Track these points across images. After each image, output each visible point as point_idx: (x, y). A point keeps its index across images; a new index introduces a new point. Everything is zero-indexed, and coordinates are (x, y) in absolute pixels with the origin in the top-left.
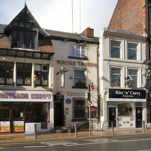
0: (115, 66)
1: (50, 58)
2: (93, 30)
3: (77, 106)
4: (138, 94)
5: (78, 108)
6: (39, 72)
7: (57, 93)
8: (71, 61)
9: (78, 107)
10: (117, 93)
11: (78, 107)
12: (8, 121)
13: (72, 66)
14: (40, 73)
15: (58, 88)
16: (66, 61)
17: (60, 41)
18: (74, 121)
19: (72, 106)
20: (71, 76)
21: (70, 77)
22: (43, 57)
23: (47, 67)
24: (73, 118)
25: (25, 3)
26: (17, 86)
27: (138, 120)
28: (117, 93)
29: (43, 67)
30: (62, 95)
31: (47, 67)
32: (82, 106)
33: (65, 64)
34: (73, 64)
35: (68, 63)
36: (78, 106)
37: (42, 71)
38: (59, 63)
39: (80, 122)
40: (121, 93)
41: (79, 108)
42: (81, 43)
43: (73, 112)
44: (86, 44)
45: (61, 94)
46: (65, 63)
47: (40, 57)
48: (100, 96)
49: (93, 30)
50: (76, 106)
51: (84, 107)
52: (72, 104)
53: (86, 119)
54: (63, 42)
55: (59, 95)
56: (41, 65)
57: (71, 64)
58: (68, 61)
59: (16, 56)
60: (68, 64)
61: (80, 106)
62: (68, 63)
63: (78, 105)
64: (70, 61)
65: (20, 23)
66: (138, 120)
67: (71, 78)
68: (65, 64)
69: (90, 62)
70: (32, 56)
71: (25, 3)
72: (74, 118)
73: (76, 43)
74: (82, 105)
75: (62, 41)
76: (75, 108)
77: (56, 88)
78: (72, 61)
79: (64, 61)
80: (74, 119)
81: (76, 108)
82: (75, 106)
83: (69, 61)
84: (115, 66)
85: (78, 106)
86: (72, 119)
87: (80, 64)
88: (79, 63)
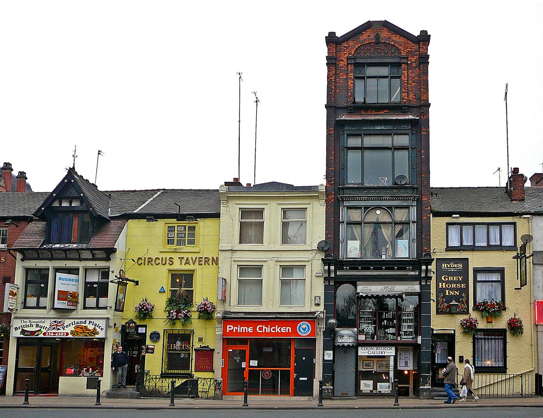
0: (237, 274)
3: (170, 345)
4: (289, 329)
5: (174, 350)
9: (173, 347)
10: (175, 348)
11: (173, 347)
12: (333, 266)
13: (168, 267)
14: (96, 286)
18: (164, 376)
25: (74, 164)
28: (175, 348)
34: (168, 262)
36: (173, 346)
51: (184, 348)
59: (51, 259)
60: (159, 263)
71: (74, 164)
84: (237, 274)
87: (184, 261)
88: (181, 262)
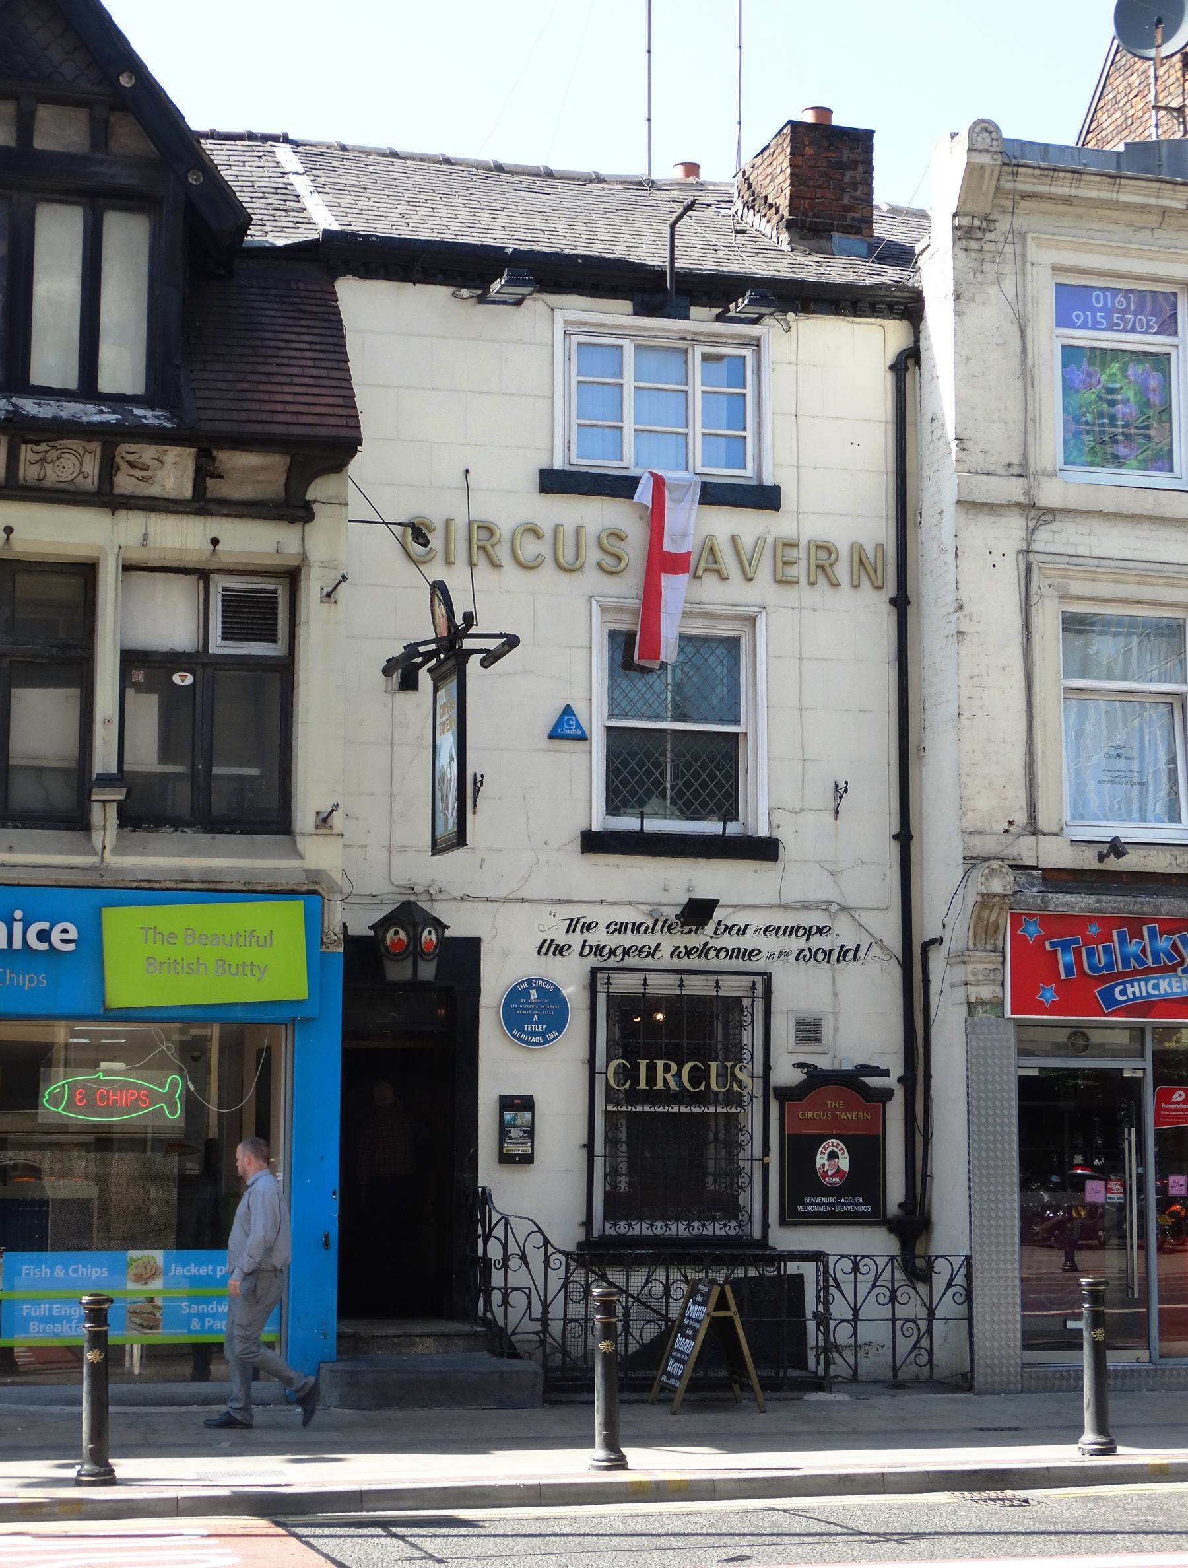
1: (309, 496)
2: (861, 141)
6: (174, 660)
7: (389, 909)
8: (569, 528)
9: (651, 1080)
11: (651, 1080)
15: (403, 850)
16: (505, 527)
17: (440, 293)
19: (582, 1073)
20: (568, 711)
21: (559, 723)
22: (216, 488)
23: (267, 602)
24: (588, 1224)
26: (119, 837)
27: (1144, 1309)
29: (232, 602)
30: (448, 933)
31: (267, 602)
32: (699, 1076)
33: (496, 566)
34: (593, 555)
35: (530, 548)
36: (652, 1069)
37: (218, 646)
38: (417, 549)
39: (660, 1275)
40: (43, 936)
41: (668, 1097)
42: (695, 311)
43: (589, 1146)
44: (755, 321)
45: (439, 926)
46: (502, 553)
47: (188, 494)
48: (926, 946)
49: (861, 141)
50: (630, 1074)
52: (583, 1052)
53: (757, 1234)
54: (482, 300)
55: (415, 938)
56: (203, 575)
57: (880, 584)
58: (534, 531)
61: (679, 1074)
62: (530, 548)
63: (652, 1056)
64: (556, 528)
65: (45, 114)
66: (1144, 1309)
67: (560, 732)
68: (496, 566)
69: (812, 529)
70: (91, 483)
72: (607, 1217)
73: (636, 313)
74: (704, 1054)
75: (465, 292)
76: (610, 1097)
77: (389, 848)
78: (578, 530)
79: (488, 529)
80: (603, 1236)
81: (634, 1096)
82: (609, 1070)
83: (546, 527)
85: (652, 1069)
86: (580, 1235)
